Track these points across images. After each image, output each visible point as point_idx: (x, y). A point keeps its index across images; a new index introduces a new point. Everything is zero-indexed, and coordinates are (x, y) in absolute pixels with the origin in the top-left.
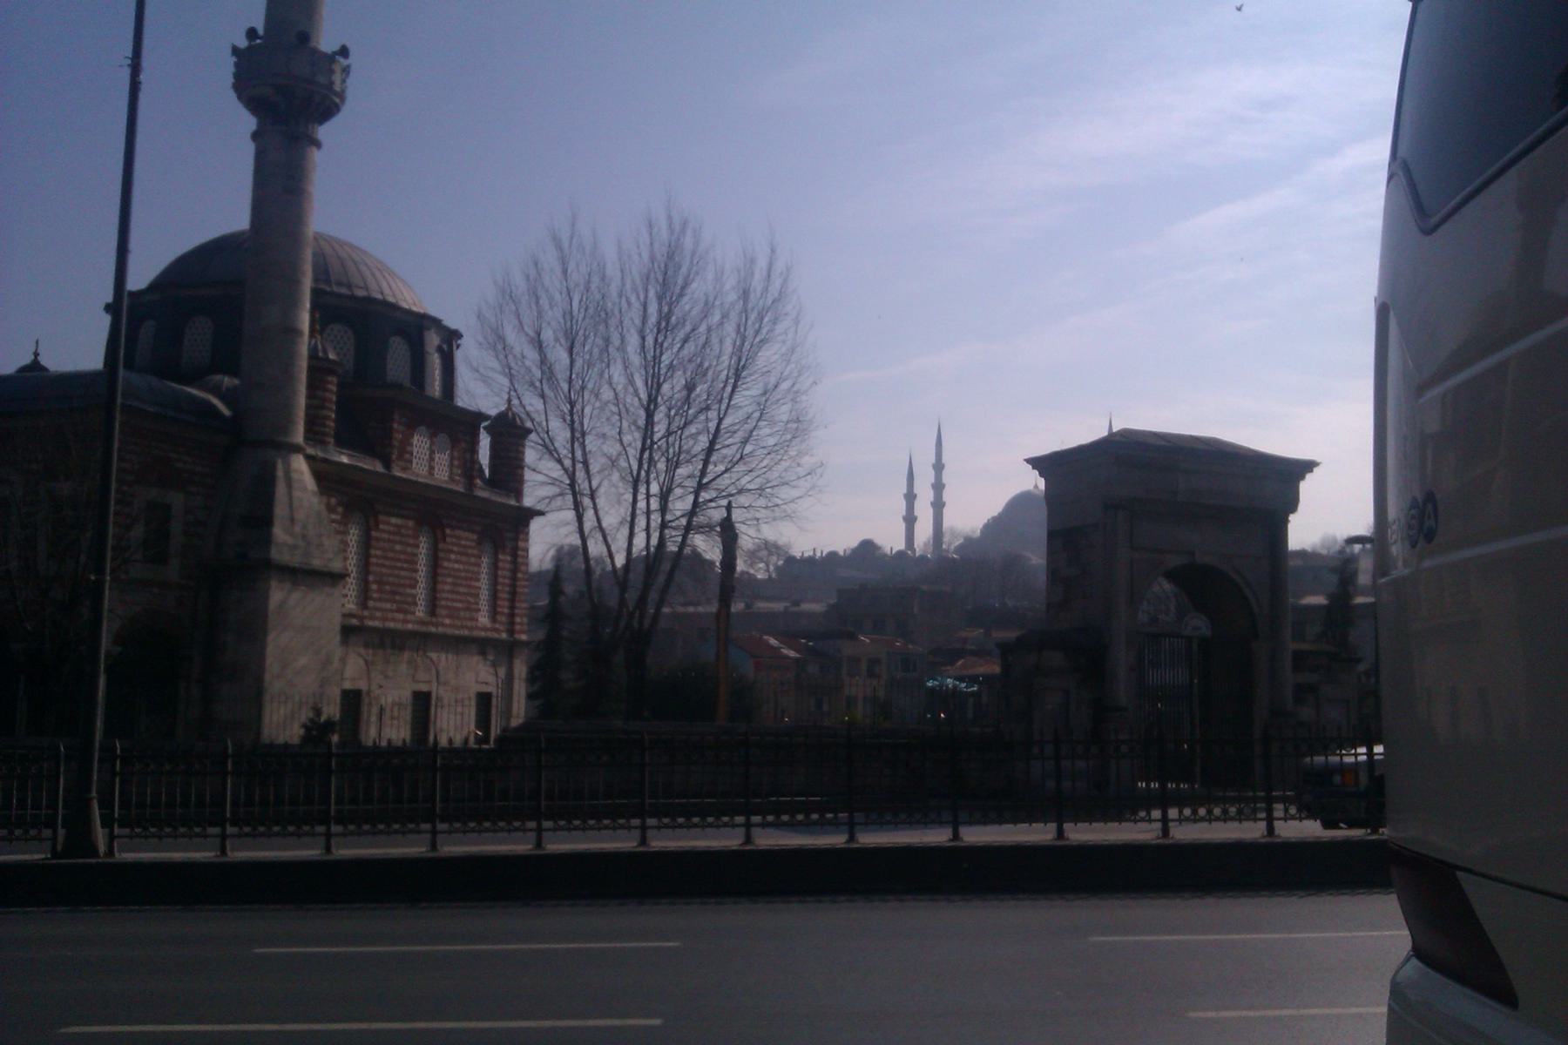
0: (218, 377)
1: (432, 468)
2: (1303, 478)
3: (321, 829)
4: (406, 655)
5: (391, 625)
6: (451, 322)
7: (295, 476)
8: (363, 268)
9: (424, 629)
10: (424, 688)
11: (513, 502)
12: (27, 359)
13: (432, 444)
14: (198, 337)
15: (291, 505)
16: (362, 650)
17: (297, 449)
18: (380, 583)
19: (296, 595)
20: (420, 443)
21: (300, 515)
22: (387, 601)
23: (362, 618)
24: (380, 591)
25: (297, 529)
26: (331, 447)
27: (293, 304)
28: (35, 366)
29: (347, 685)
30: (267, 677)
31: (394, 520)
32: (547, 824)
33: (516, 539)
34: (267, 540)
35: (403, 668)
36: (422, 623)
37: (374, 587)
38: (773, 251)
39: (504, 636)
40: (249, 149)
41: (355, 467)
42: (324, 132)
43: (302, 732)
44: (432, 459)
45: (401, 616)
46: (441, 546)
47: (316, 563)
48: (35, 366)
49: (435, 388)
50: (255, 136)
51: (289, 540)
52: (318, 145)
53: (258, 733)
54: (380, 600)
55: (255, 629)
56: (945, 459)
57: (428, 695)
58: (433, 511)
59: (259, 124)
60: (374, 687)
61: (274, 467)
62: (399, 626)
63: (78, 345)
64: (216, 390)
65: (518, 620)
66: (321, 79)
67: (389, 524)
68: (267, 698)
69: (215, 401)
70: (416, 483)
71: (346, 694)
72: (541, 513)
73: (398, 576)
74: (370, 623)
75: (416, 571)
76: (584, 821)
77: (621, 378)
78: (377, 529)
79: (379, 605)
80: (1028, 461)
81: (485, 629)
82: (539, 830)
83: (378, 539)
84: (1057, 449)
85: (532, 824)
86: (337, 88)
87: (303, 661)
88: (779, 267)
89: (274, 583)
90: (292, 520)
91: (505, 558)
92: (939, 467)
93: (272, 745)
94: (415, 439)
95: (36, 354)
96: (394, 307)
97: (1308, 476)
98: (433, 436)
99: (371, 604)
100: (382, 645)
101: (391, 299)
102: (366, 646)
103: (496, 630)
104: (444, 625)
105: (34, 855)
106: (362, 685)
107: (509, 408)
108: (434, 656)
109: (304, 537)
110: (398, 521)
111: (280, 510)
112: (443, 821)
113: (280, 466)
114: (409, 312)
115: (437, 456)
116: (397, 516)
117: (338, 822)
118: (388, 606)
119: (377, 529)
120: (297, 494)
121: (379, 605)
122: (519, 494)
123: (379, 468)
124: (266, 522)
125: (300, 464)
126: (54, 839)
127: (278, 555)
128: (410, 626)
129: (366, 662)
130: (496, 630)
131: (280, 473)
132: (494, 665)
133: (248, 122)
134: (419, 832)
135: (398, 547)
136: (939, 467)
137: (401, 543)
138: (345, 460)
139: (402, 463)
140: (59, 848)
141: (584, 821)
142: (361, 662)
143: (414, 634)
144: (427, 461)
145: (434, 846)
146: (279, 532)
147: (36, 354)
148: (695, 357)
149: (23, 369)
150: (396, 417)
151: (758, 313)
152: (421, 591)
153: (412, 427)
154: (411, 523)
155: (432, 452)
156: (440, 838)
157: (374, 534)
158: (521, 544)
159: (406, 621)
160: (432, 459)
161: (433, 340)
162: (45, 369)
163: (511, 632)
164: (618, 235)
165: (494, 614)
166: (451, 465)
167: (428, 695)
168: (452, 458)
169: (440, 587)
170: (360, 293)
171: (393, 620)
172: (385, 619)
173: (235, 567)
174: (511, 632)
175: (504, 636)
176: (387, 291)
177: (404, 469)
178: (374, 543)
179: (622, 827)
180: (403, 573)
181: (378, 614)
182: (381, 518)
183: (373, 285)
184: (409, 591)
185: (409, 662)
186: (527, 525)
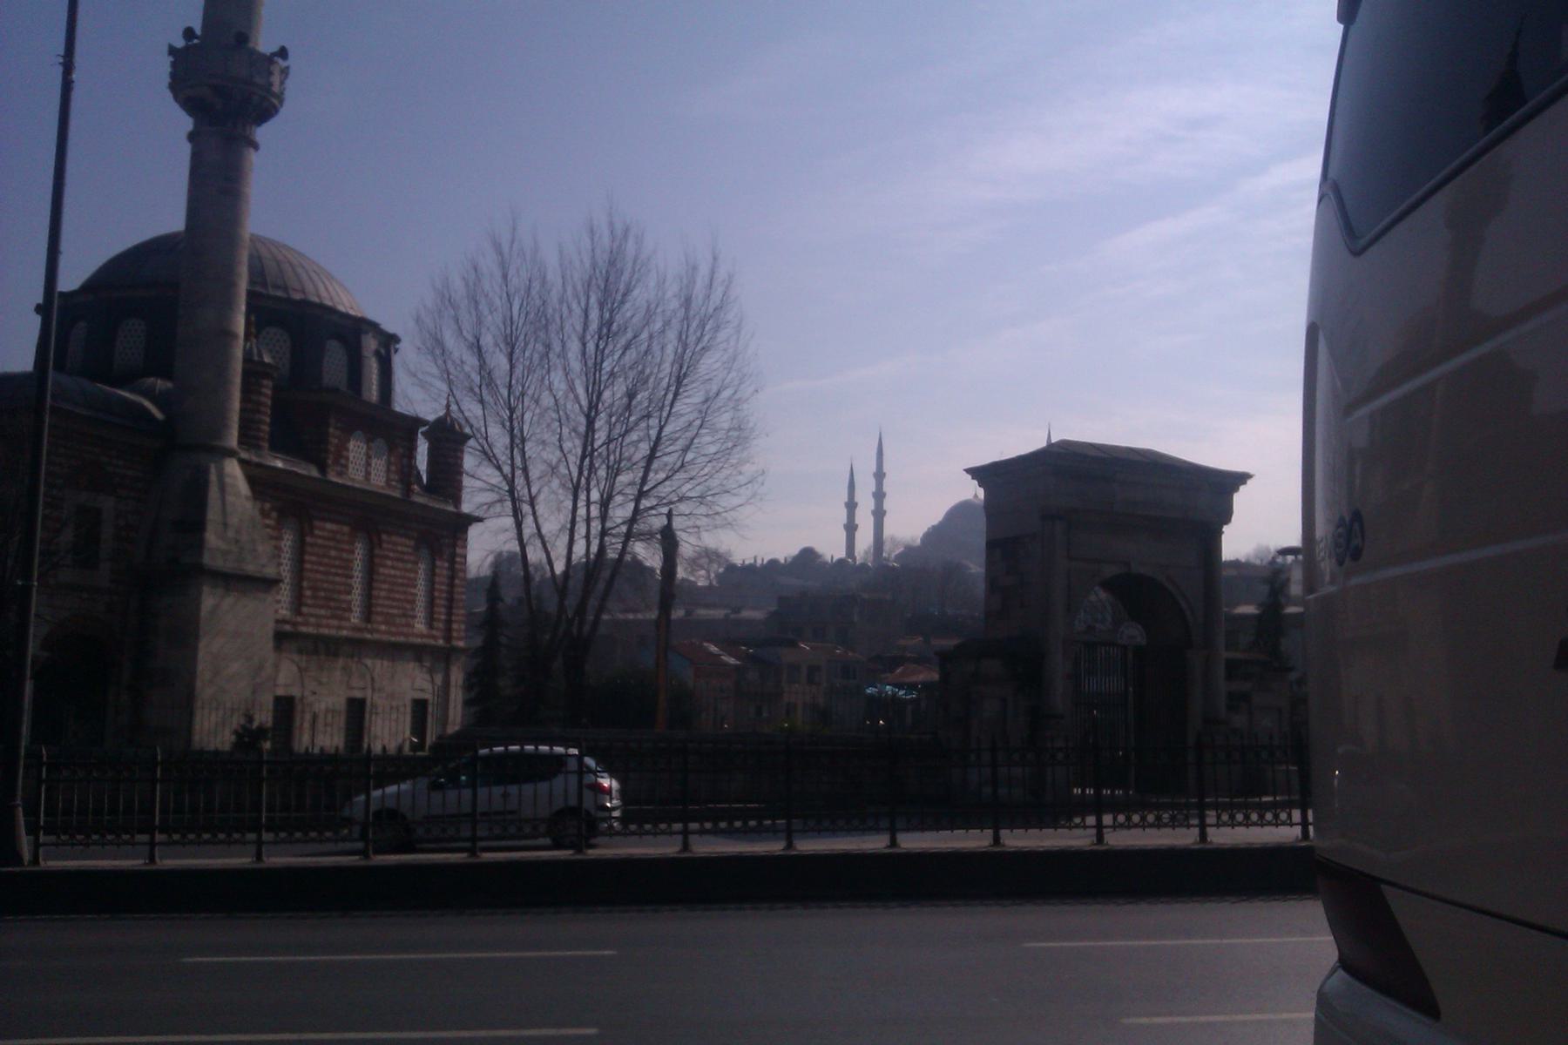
1: (368, 474)
2: (1236, 489)
4: (341, 662)
5: (325, 631)
6: (389, 326)
7: (228, 480)
8: (300, 270)
9: (357, 635)
10: (358, 694)
11: (451, 508)
13: (369, 448)
14: (131, 340)
16: (296, 657)
17: (231, 453)
18: (314, 589)
19: (229, 601)
20: (356, 448)
21: (234, 521)
22: (322, 607)
23: (294, 624)
24: (315, 597)
25: (231, 534)
27: (228, 303)
29: (280, 692)
30: (199, 684)
31: (329, 526)
33: (454, 546)
34: (200, 545)
36: (359, 630)
39: (441, 642)
40: (186, 149)
45: (334, 622)
46: (377, 551)
47: (250, 568)
50: (192, 137)
51: (223, 546)
52: (256, 146)
53: (189, 741)
55: (186, 635)
56: (886, 469)
58: (369, 517)
59: (196, 125)
61: (206, 471)
62: (333, 632)
64: (148, 394)
66: (258, 80)
67: (323, 529)
68: (199, 704)
69: (147, 404)
70: (354, 488)
74: (304, 629)
86: (276, 89)
89: (206, 589)
90: (225, 525)
92: (880, 476)
93: (202, 752)
94: (351, 445)
96: (332, 311)
97: (1242, 488)
98: (369, 441)
99: (305, 610)
101: (328, 303)
102: (300, 652)
103: (434, 637)
104: (378, 631)
106: (295, 692)
108: (369, 662)
109: (237, 541)
111: (213, 514)
113: (213, 470)
114: (346, 316)
115: (374, 461)
117: (269, 830)
118: (323, 612)
119: (312, 535)
120: (230, 499)
121: (312, 611)
122: (457, 501)
123: (314, 473)
124: (199, 526)
125: (233, 469)
128: (345, 633)
129: (300, 670)
130: (434, 637)
131: (213, 477)
132: (431, 672)
135: (333, 553)
136: (880, 476)
138: (280, 464)
142: (295, 669)
143: (348, 640)
144: (363, 466)
146: (211, 538)
148: (636, 362)
151: (700, 320)
152: (356, 597)
153: (348, 432)
154: (346, 529)
155: (369, 457)
156: (692, 838)
157: (308, 539)
158: (459, 551)
159: (340, 628)
160: (368, 464)
161: (370, 344)
163: (448, 638)
164: (558, 239)
165: (431, 620)
166: (388, 470)
168: (389, 464)
169: (375, 593)
171: (328, 626)
172: (318, 626)
173: (166, 570)
174: (448, 638)
175: (441, 642)
177: (340, 474)
178: (309, 549)
181: (312, 620)
182: (317, 523)
183: (309, 287)
184: (343, 597)
185: (344, 669)
186: (466, 532)
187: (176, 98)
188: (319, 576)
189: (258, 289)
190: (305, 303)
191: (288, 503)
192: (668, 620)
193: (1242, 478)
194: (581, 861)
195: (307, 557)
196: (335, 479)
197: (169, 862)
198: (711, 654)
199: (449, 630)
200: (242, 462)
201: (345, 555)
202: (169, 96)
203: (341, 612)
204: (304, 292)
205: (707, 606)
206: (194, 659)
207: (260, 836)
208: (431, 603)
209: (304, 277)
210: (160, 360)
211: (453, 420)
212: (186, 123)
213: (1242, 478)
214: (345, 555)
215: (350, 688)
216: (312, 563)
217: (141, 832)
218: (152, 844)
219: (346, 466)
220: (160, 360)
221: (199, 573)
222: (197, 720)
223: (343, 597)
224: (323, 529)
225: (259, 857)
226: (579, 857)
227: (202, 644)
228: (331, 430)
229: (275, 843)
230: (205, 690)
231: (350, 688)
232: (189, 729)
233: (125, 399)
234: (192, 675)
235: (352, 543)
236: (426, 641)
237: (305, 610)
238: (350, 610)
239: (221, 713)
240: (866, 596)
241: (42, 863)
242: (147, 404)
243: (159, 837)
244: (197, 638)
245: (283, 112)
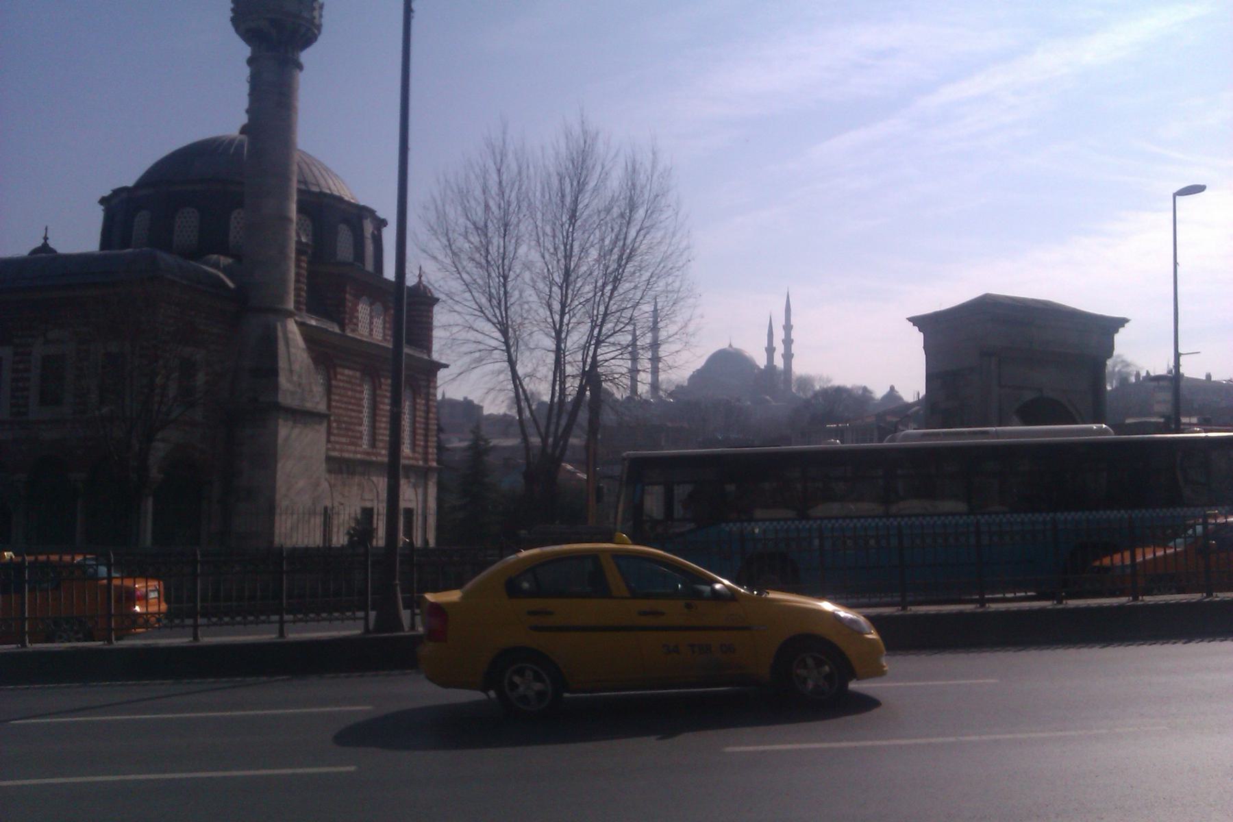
0: (215, 257)
1: (371, 330)
2: (1117, 331)
3: (189, 621)
4: (357, 479)
5: (346, 455)
6: (381, 214)
7: (290, 336)
8: (314, 169)
9: (367, 458)
10: (368, 505)
11: (426, 357)
12: (39, 243)
13: (371, 311)
14: (187, 225)
15: (289, 360)
17: (290, 314)
19: (296, 431)
20: (363, 310)
21: (296, 367)
22: (343, 436)
24: (338, 428)
25: (295, 378)
26: (304, 313)
27: (286, 197)
28: (45, 248)
30: (278, 497)
31: (347, 372)
32: (287, 617)
33: (428, 387)
34: (276, 387)
35: (355, 489)
36: (368, 454)
37: (334, 425)
38: (654, 153)
39: (421, 463)
40: (246, 71)
41: (322, 329)
42: (305, 56)
43: (346, 539)
44: (371, 323)
45: (353, 448)
46: (378, 392)
47: (309, 405)
48: (45, 248)
49: (370, 266)
50: (250, 62)
53: (272, 542)
54: (339, 435)
55: (267, 459)
56: (793, 321)
57: (372, 509)
58: (370, 362)
59: (253, 52)
60: (336, 504)
61: (275, 329)
62: (351, 456)
63: (80, 235)
64: (216, 265)
65: (430, 450)
66: (305, 14)
67: (343, 374)
68: (278, 511)
69: (222, 275)
70: (361, 341)
71: (326, 509)
72: (446, 366)
73: (351, 417)
75: (361, 412)
76: (233, 618)
77: (531, 257)
78: (336, 379)
79: (337, 439)
80: (910, 319)
81: (409, 458)
82: (282, 622)
83: (339, 387)
84: (938, 309)
85: (275, 618)
86: (317, 21)
87: (301, 484)
88: (660, 167)
89: (281, 422)
90: (291, 372)
91: (421, 401)
92: (788, 328)
93: (281, 549)
94: (360, 307)
95: (46, 239)
96: (340, 199)
97: (1121, 330)
98: (371, 304)
99: (332, 438)
100: (340, 472)
101: (336, 193)
103: (416, 459)
104: (380, 454)
105: (352, 630)
107: (420, 282)
108: (374, 479)
109: (300, 385)
110: (351, 373)
111: (282, 363)
112: (288, 613)
113: (279, 328)
114: (349, 203)
115: (375, 320)
116: (349, 368)
117: (203, 616)
118: (344, 440)
119: (336, 379)
120: (293, 350)
121: (337, 439)
122: (429, 350)
123: (337, 330)
124: (273, 372)
125: (292, 326)
126: (366, 618)
127: (284, 399)
128: (359, 456)
130: (416, 459)
131: (280, 334)
132: (415, 487)
133: (244, 50)
134: (270, 622)
135: (350, 393)
136: (788, 328)
137: (352, 390)
138: (313, 323)
139: (352, 326)
140: (371, 627)
141: (233, 618)
144: (370, 325)
145: (281, 633)
146: (283, 381)
147: (46, 239)
148: (598, 236)
149: (36, 251)
150: (348, 288)
151: (635, 208)
152: (365, 428)
153: (357, 297)
154: (358, 374)
155: (371, 317)
156: (286, 626)
157: (334, 382)
158: (432, 391)
159: (355, 452)
160: (371, 323)
161: (369, 228)
162: (53, 251)
163: (426, 460)
164: (542, 143)
165: (414, 445)
166: (384, 328)
167: (372, 509)
168: (385, 322)
169: (378, 424)
170: (315, 189)
171: (348, 451)
172: (341, 451)
173: (249, 406)
174: (426, 460)
175: (421, 463)
176: (333, 187)
177: (353, 331)
178: (334, 390)
179: (348, 618)
180: (353, 414)
181: (338, 447)
182: (339, 370)
183: (322, 182)
184: (357, 428)
185: (359, 485)
186: (435, 375)
187: (237, 30)
188: (341, 411)
189: (303, 187)
190: (321, 195)
191: (327, 355)
192: (566, 441)
193: (1122, 322)
194: (1063, 609)
195: (333, 397)
196: (350, 335)
197: (208, 639)
198: (569, 471)
199: (426, 453)
200: (301, 325)
201: (358, 395)
202: (232, 30)
203: (355, 440)
204: (318, 185)
205: (1132, 416)
206: (273, 478)
207: (282, 618)
208: (414, 433)
209: (317, 173)
210: (213, 240)
211: (425, 287)
212: (246, 51)
213: (1122, 322)
214: (358, 395)
215: (363, 499)
216: (337, 401)
217: (188, 617)
218: (282, 622)
219: (356, 325)
220: (213, 240)
221: (279, 409)
222: (277, 525)
223: (357, 428)
224: (343, 374)
225: (196, 638)
226: (1060, 606)
227: (279, 465)
228: (348, 296)
229: (294, 622)
230: (282, 503)
231: (363, 499)
232: (272, 534)
233: (206, 272)
234: (273, 489)
235: (361, 385)
236: (411, 462)
237: (332, 438)
238: (361, 438)
239: (295, 517)
240: (669, 424)
241: (28, 645)
242: (222, 275)
243: (200, 621)
244: (276, 462)
245: (321, 40)
